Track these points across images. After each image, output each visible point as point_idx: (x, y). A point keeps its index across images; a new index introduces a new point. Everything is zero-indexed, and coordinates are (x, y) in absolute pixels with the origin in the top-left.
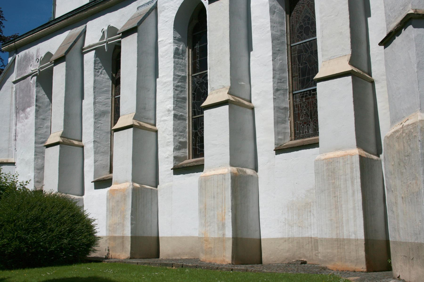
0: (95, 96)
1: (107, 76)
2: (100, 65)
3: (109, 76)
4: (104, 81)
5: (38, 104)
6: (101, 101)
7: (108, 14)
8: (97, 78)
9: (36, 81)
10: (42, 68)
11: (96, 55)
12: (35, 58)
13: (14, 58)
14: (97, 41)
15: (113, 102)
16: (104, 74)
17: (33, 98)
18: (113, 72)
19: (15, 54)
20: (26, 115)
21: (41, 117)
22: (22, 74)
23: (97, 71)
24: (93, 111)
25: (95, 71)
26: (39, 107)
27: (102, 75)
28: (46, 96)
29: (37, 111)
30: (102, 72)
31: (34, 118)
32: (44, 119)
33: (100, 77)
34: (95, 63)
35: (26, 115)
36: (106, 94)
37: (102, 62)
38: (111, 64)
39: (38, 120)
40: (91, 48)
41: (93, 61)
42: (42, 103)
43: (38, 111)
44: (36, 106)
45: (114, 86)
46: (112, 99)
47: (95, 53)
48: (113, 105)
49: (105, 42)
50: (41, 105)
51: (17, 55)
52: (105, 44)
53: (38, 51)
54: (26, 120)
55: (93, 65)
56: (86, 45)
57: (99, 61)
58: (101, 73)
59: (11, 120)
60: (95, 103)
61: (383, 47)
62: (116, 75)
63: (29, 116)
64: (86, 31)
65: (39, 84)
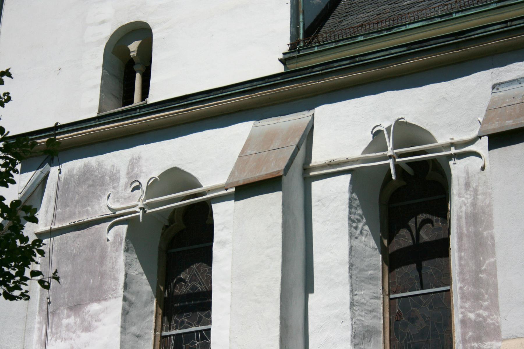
0: (352, 286)
1: (372, 243)
2: (360, 212)
3: (376, 242)
4: (367, 253)
5: (128, 296)
6: (363, 301)
7: (388, 92)
8: (355, 243)
9: (127, 237)
10: (151, 206)
11: (354, 187)
12: (123, 180)
13: (43, 175)
14: (357, 153)
15: (387, 308)
16: (366, 235)
17: (116, 279)
18: (384, 236)
19: (47, 166)
20: (83, 320)
21: (134, 329)
22: (72, 215)
23: (354, 225)
24: (348, 323)
25: (350, 226)
26: (131, 304)
27: (363, 238)
28: (144, 277)
29: (125, 313)
30: (362, 229)
31: (119, 329)
32: (138, 336)
33: (361, 242)
34: (350, 206)
35: (83, 320)
36: (370, 286)
37: (363, 206)
38: (378, 214)
39: (128, 337)
40: (332, 169)
41: (347, 201)
42: (137, 294)
43: (128, 313)
44: (125, 299)
45: (386, 268)
46: (383, 298)
47: (352, 182)
48: (387, 315)
49: (390, 157)
50: (133, 298)
51: (54, 170)
52: (391, 162)
53: (133, 163)
54: (85, 336)
55: (347, 210)
56: (317, 159)
57: (357, 202)
58: (361, 233)
59: (27, 331)
60: (352, 305)
61: (10, 71)
62: (389, 243)
63: (95, 324)
64: (313, 127)
65: (131, 245)
